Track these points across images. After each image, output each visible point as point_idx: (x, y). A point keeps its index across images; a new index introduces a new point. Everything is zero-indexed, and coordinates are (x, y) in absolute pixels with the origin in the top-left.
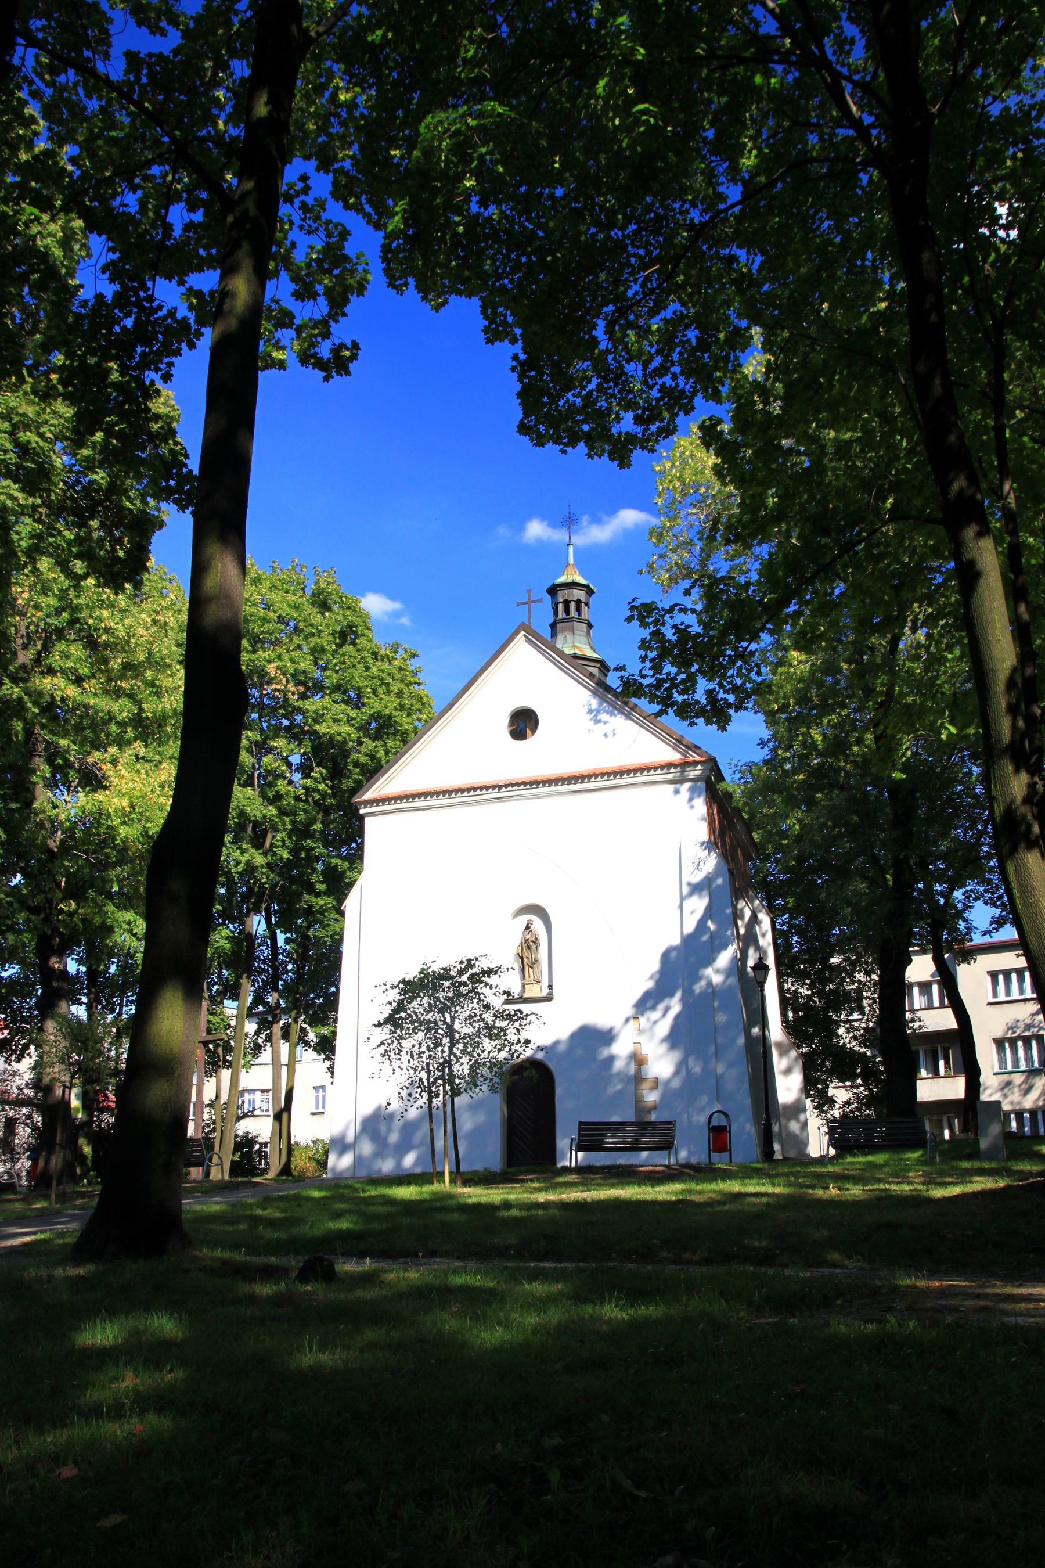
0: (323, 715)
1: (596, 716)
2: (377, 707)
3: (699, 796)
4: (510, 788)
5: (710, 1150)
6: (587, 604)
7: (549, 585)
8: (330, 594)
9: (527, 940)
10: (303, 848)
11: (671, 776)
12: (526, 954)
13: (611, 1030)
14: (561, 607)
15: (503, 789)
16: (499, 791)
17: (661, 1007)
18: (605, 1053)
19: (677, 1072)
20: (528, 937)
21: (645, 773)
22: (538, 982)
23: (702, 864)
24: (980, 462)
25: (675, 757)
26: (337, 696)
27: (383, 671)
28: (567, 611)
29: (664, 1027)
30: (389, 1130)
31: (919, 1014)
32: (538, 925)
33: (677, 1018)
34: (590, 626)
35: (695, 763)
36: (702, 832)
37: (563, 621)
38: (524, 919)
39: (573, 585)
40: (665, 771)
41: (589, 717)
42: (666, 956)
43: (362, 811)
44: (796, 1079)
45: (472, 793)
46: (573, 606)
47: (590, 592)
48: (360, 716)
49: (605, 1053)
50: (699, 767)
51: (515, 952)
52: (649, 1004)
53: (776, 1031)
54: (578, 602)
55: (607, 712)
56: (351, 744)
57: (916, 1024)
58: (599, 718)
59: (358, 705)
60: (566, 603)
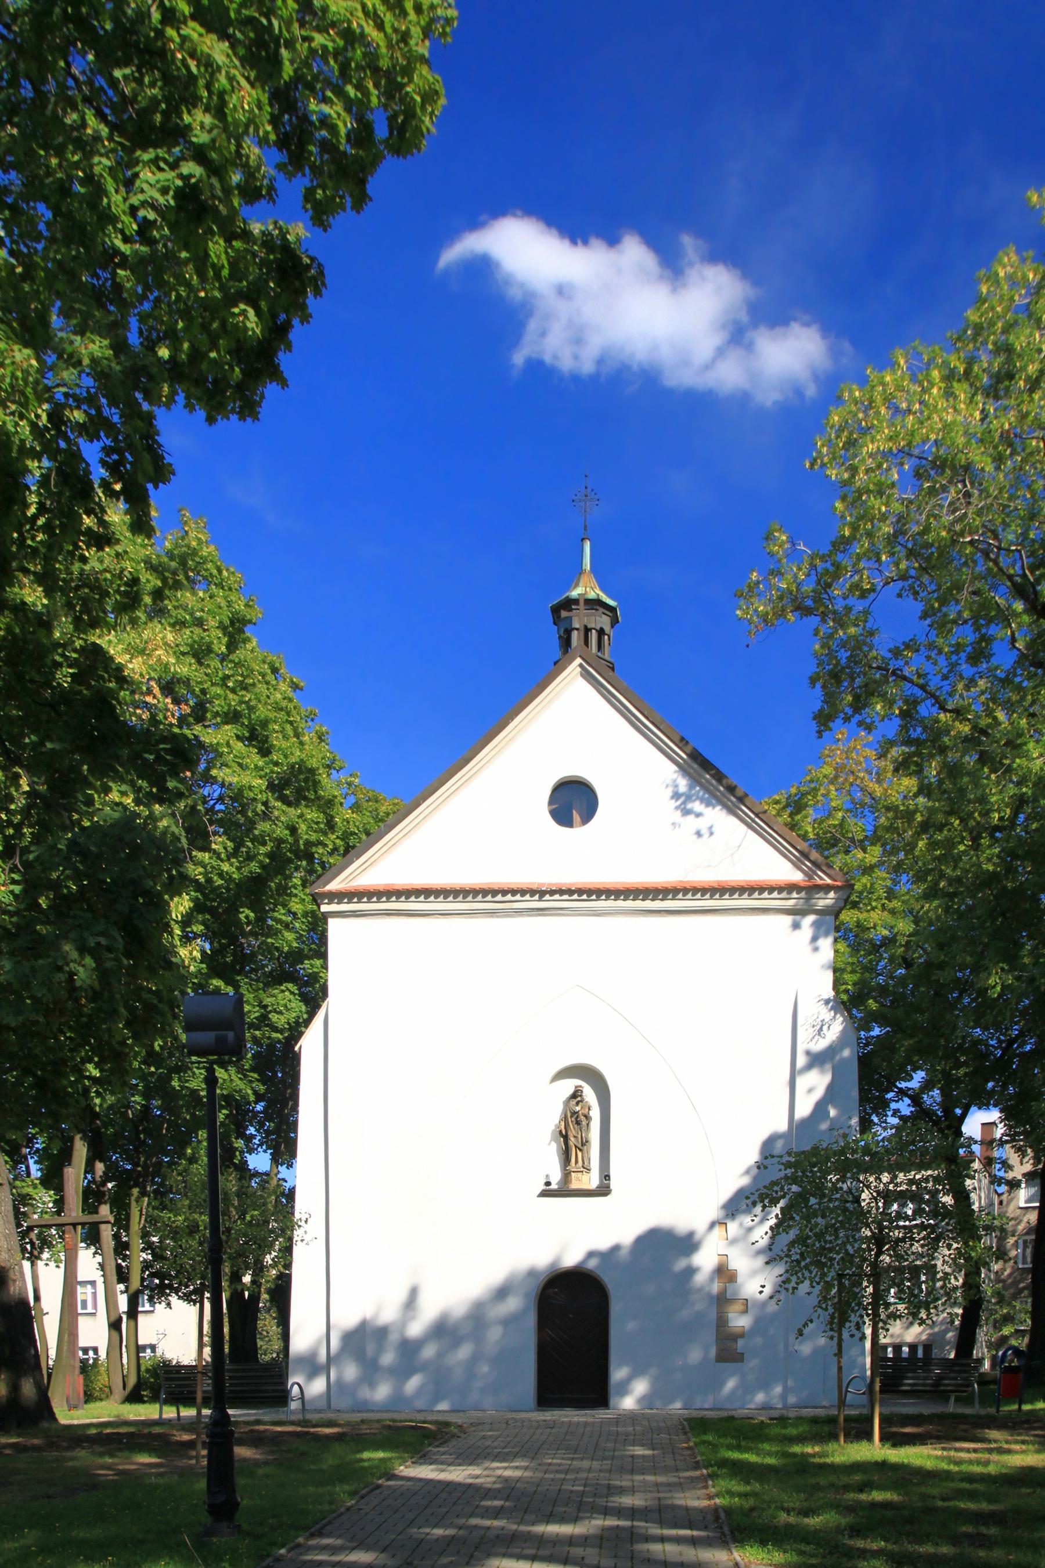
1: (684, 803)
2: (297, 755)
3: (826, 935)
4: (557, 897)
11: (791, 902)
13: (691, 1235)
15: (547, 897)
16: (540, 900)
18: (681, 1264)
23: (825, 1028)
25: (797, 877)
32: (590, 1095)
35: (827, 888)
38: (569, 1085)
39: (595, 604)
40: (784, 895)
41: (674, 804)
43: (324, 908)
45: (499, 898)
46: (594, 636)
50: (832, 894)
54: (601, 632)
55: (702, 800)
58: (689, 806)
59: (265, 751)
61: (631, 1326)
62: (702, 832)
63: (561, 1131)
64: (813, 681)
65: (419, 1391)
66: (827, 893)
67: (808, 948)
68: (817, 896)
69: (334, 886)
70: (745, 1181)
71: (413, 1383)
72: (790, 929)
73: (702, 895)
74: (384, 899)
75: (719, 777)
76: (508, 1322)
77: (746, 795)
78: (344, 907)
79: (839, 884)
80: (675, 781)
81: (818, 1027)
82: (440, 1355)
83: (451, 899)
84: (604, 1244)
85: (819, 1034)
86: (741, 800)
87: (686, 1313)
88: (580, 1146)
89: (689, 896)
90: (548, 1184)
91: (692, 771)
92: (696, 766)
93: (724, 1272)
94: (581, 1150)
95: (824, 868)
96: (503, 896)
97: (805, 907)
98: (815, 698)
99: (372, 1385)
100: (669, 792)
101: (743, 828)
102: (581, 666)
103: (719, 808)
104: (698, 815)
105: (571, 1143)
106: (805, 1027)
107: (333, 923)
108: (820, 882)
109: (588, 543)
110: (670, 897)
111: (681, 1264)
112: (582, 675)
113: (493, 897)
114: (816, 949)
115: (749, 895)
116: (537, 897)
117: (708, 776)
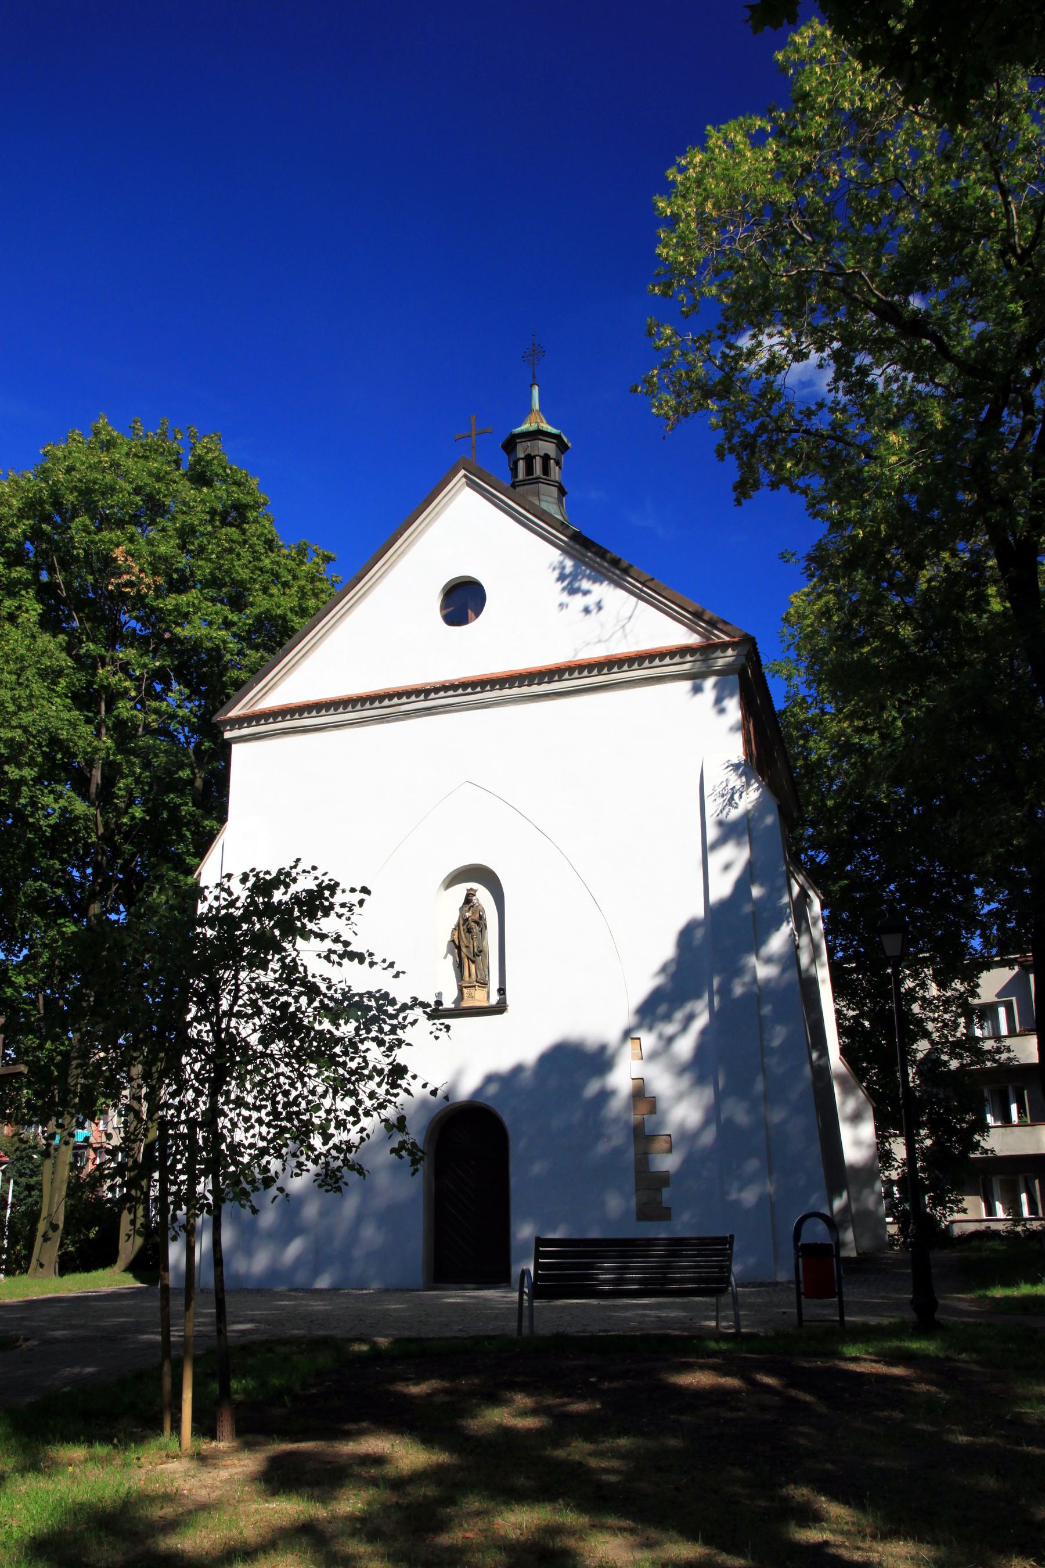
0: (188, 613)
1: (570, 583)
3: (731, 695)
4: (442, 694)
5: (799, 1294)
6: (558, 463)
7: (505, 437)
8: (209, 463)
9: (466, 920)
10: (165, 806)
11: (687, 666)
12: (464, 942)
13: (603, 1048)
14: (521, 464)
15: (432, 695)
17: (679, 1015)
18: (592, 1088)
19: (706, 1123)
20: (468, 914)
21: (646, 664)
22: (484, 984)
23: (736, 796)
25: (693, 639)
26: (211, 592)
27: (278, 563)
28: (530, 470)
29: (685, 1046)
31: (1008, 1042)
32: (484, 897)
33: (704, 1032)
34: (562, 492)
35: (724, 646)
36: (735, 749)
37: (524, 483)
38: (460, 891)
39: (538, 434)
40: (677, 659)
41: (560, 586)
42: (686, 936)
43: (227, 735)
44: (867, 1130)
45: (386, 702)
46: (538, 464)
47: (562, 447)
48: (244, 619)
50: (730, 652)
51: (449, 938)
52: (662, 1009)
53: (836, 1061)
54: (546, 458)
55: (589, 578)
56: (228, 657)
57: (1004, 1056)
58: (576, 585)
60: (529, 459)
61: (537, 1168)
63: (453, 941)
64: (720, 454)
65: (298, 1262)
66: (724, 651)
68: (714, 655)
69: (233, 713)
70: (658, 981)
71: (295, 1248)
72: (691, 694)
73: (589, 672)
74: (280, 719)
75: (602, 553)
77: (631, 566)
78: (245, 731)
79: (736, 640)
80: (562, 562)
81: (729, 796)
83: (341, 710)
84: (504, 1063)
85: (730, 804)
86: (626, 571)
87: (602, 1148)
88: (471, 957)
89: (576, 674)
91: (573, 552)
92: (577, 547)
93: (640, 1093)
94: (473, 962)
95: (720, 626)
96: (390, 700)
98: (731, 470)
99: (249, 1253)
100: (556, 574)
101: (633, 599)
102: (465, 476)
103: (606, 583)
104: (586, 593)
105: (463, 955)
106: (712, 798)
107: (236, 749)
108: (717, 640)
109: (537, 388)
110: (556, 678)
111: (592, 1088)
112: (468, 485)
113: (380, 702)
114: (722, 711)
115: (639, 665)
116: (422, 697)
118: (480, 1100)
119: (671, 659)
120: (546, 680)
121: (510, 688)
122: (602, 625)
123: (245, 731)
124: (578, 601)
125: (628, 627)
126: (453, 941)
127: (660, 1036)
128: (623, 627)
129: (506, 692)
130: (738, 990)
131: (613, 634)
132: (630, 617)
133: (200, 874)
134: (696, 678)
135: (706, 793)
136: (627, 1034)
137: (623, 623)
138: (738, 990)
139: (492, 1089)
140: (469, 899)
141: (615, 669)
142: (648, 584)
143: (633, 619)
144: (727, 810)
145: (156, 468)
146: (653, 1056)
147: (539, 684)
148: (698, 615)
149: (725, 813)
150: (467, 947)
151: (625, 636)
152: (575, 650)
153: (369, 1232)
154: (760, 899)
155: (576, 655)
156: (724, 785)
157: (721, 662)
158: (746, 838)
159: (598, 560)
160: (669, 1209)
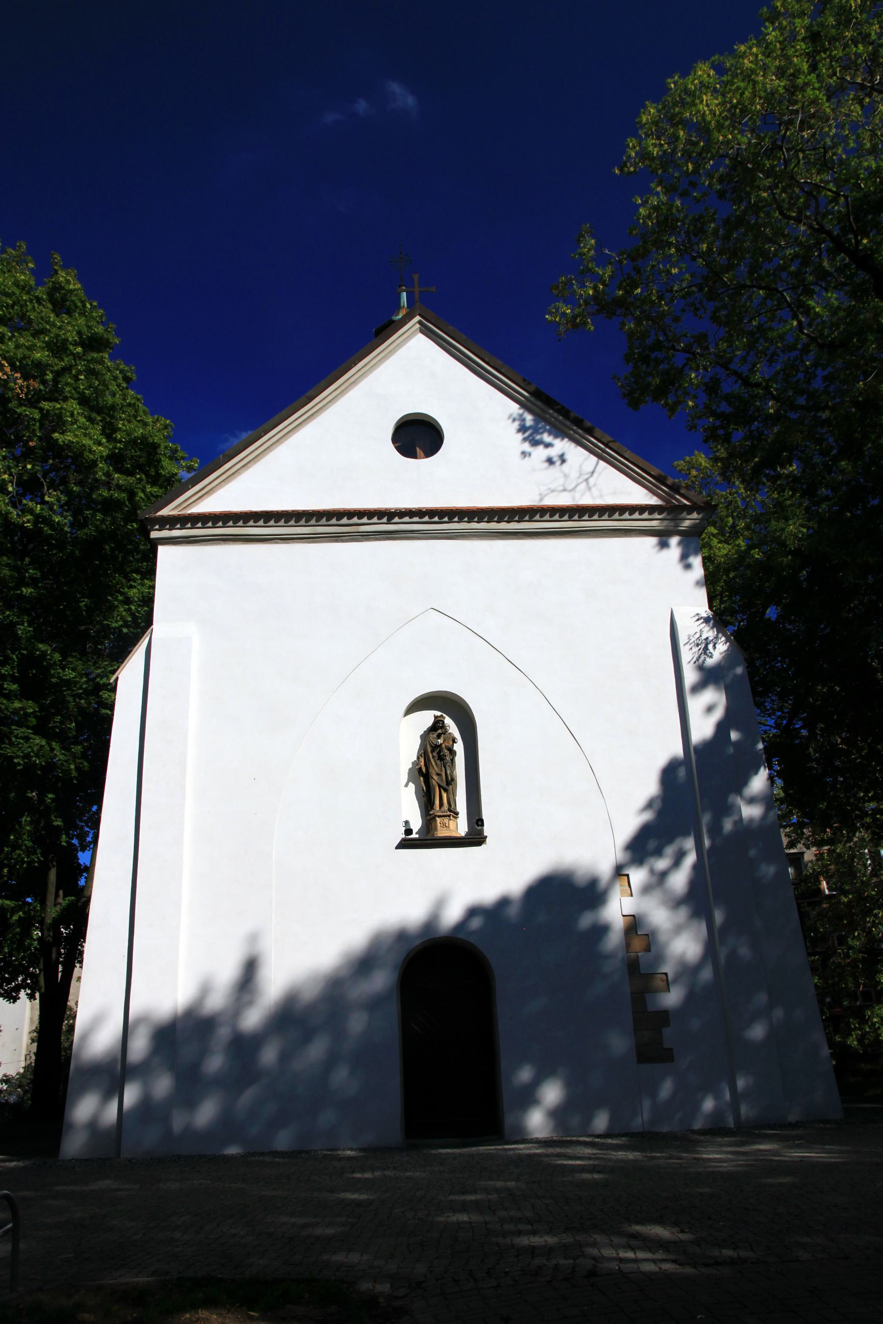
1: (531, 435)
4: (407, 519)
11: (654, 523)
12: (435, 768)
13: (593, 883)
15: (396, 520)
16: (389, 523)
17: (670, 850)
18: (586, 921)
21: (616, 516)
23: (710, 647)
24: (579, 1153)
29: (679, 880)
30: (204, 1052)
38: (427, 718)
40: (646, 515)
41: (520, 436)
42: (669, 773)
43: (154, 535)
45: (345, 521)
49: (586, 921)
50: (695, 515)
52: (652, 844)
55: (550, 434)
58: (538, 437)
62: (555, 459)
67: (679, 568)
69: (165, 512)
70: (647, 816)
71: (248, 1096)
72: (658, 548)
73: (561, 517)
76: (374, 1004)
78: (176, 533)
80: (521, 415)
81: (703, 646)
82: (285, 1057)
85: (705, 653)
86: (590, 431)
88: (444, 785)
89: (547, 517)
90: (408, 831)
91: (535, 408)
92: (539, 403)
94: (446, 790)
95: (683, 491)
97: (671, 528)
100: (516, 424)
101: (594, 459)
102: (420, 322)
104: (548, 445)
106: (688, 647)
110: (527, 518)
112: (421, 332)
116: (385, 520)
117: (551, 411)
118: (461, 936)
119: (640, 514)
120: (517, 518)
121: (478, 522)
122: (566, 476)
123: (176, 533)
124: (541, 453)
125: (592, 481)
126: (420, 769)
127: (652, 871)
128: (587, 480)
129: (474, 525)
130: (728, 825)
131: (577, 485)
132: (593, 472)
133: (117, 679)
134: (663, 537)
135: (682, 639)
136: (619, 872)
137: (586, 477)
138: (728, 825)
139: (476, 923)
140: (437, 726)
141: (586, 517)
142: (610, 445)
143: (595, 475)
144: (703, 657)
145: (23, 280)
146: (646, 890)
147: (508, 522)
148: (661, 479)
149: (701, 660)
150: (438, 774)
151: (589, 489)
152: (540, 495)
153: (341, 1075)
154: (737, 744)
155: (541, 500)
156: (698, 635)
157: (687, 523)
158: (723, 686)
159: (561, 418)
160: (671, 1050)
